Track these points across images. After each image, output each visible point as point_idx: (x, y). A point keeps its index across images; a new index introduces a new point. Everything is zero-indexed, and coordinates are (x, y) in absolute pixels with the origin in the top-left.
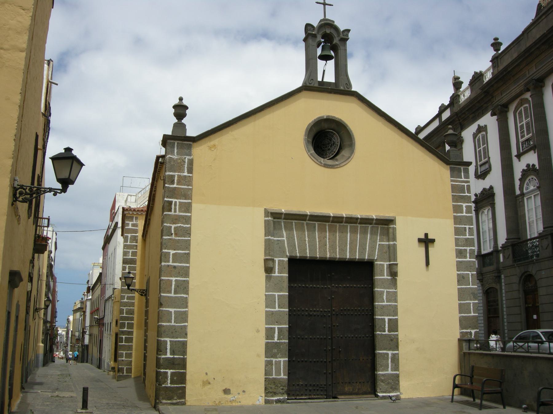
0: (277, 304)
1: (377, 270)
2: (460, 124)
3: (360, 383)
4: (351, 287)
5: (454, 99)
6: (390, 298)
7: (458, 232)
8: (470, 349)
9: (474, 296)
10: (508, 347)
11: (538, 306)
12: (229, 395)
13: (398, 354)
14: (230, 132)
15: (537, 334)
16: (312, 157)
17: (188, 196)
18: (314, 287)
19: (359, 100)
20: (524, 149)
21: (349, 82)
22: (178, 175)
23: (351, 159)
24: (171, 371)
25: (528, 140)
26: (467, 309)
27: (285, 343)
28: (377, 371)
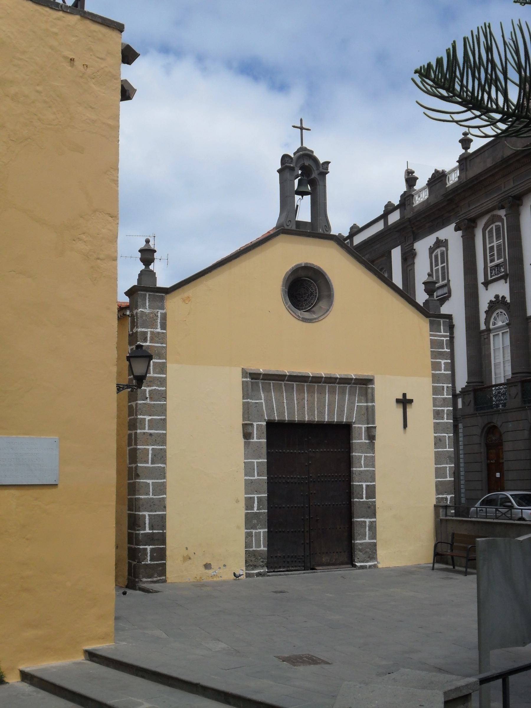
0: (256, 472)
1: (355, 433)
2: (413, 232)
3: (337, 552)
4: (328, 452)
5: (406, 200)
6: (368, 463)
7: (436, 391)
8: (446, 516)
9: (450, 460)
10: (472, 512)
11: (503, 463)
12: (210, 570)
13: (375, 522)
14: (205, 282)
15: (506, 496)
16: (290, 310)
17: (162, 355)
18: (292, 453)
19: (338, 245)
20: (493, 275)
21: (328, 223)
22: (151, 331)
23: (330, 312)
24: (151, 547)
25: (498, 266)
26: (443, 474)
27: (264, 513)
28: (354, 540)
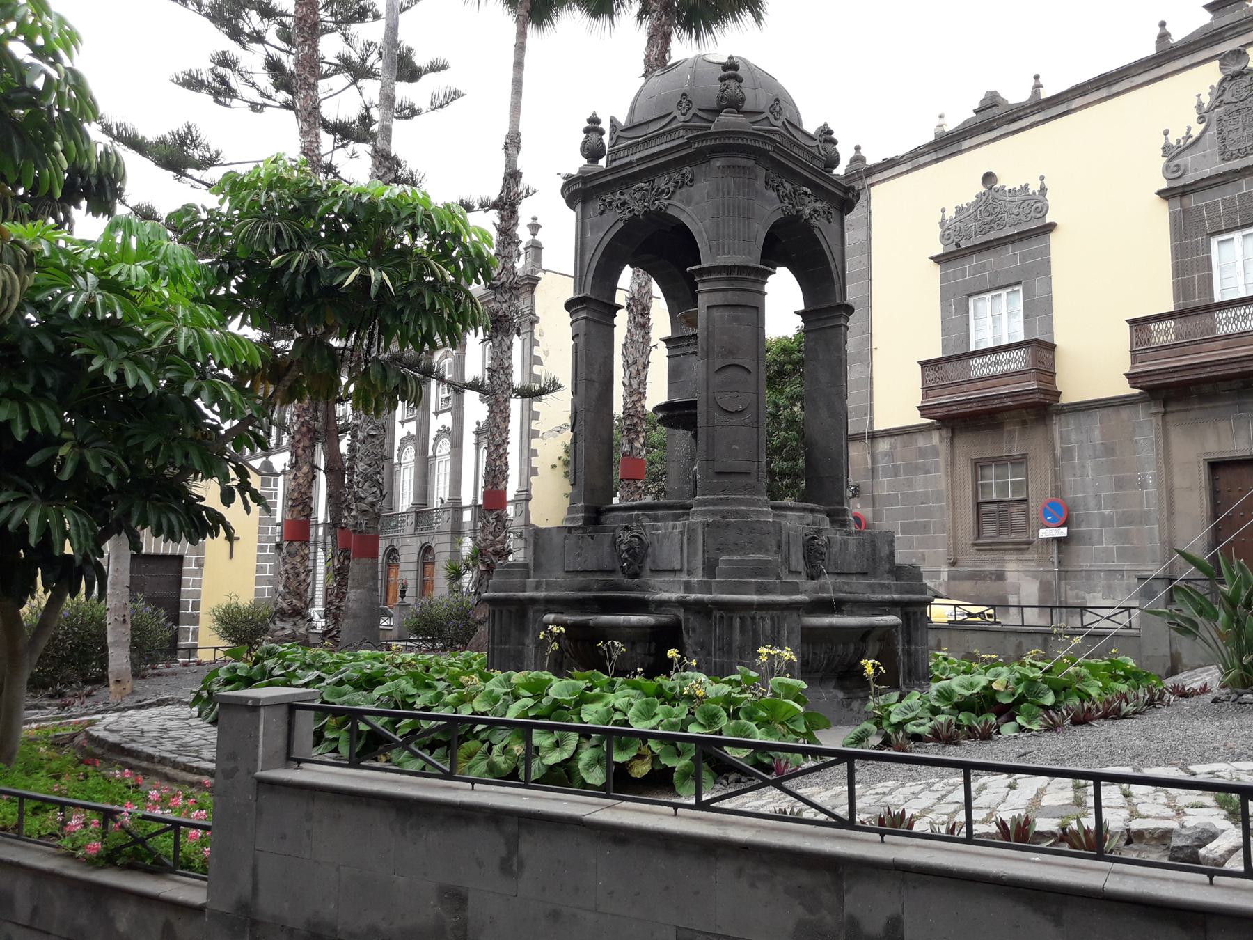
1: (186, 562)
